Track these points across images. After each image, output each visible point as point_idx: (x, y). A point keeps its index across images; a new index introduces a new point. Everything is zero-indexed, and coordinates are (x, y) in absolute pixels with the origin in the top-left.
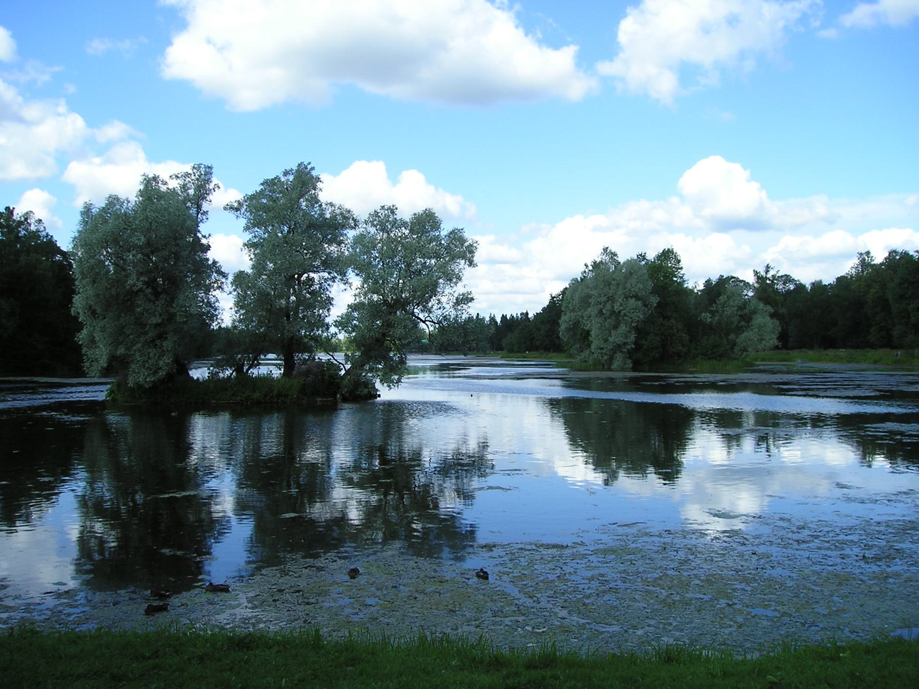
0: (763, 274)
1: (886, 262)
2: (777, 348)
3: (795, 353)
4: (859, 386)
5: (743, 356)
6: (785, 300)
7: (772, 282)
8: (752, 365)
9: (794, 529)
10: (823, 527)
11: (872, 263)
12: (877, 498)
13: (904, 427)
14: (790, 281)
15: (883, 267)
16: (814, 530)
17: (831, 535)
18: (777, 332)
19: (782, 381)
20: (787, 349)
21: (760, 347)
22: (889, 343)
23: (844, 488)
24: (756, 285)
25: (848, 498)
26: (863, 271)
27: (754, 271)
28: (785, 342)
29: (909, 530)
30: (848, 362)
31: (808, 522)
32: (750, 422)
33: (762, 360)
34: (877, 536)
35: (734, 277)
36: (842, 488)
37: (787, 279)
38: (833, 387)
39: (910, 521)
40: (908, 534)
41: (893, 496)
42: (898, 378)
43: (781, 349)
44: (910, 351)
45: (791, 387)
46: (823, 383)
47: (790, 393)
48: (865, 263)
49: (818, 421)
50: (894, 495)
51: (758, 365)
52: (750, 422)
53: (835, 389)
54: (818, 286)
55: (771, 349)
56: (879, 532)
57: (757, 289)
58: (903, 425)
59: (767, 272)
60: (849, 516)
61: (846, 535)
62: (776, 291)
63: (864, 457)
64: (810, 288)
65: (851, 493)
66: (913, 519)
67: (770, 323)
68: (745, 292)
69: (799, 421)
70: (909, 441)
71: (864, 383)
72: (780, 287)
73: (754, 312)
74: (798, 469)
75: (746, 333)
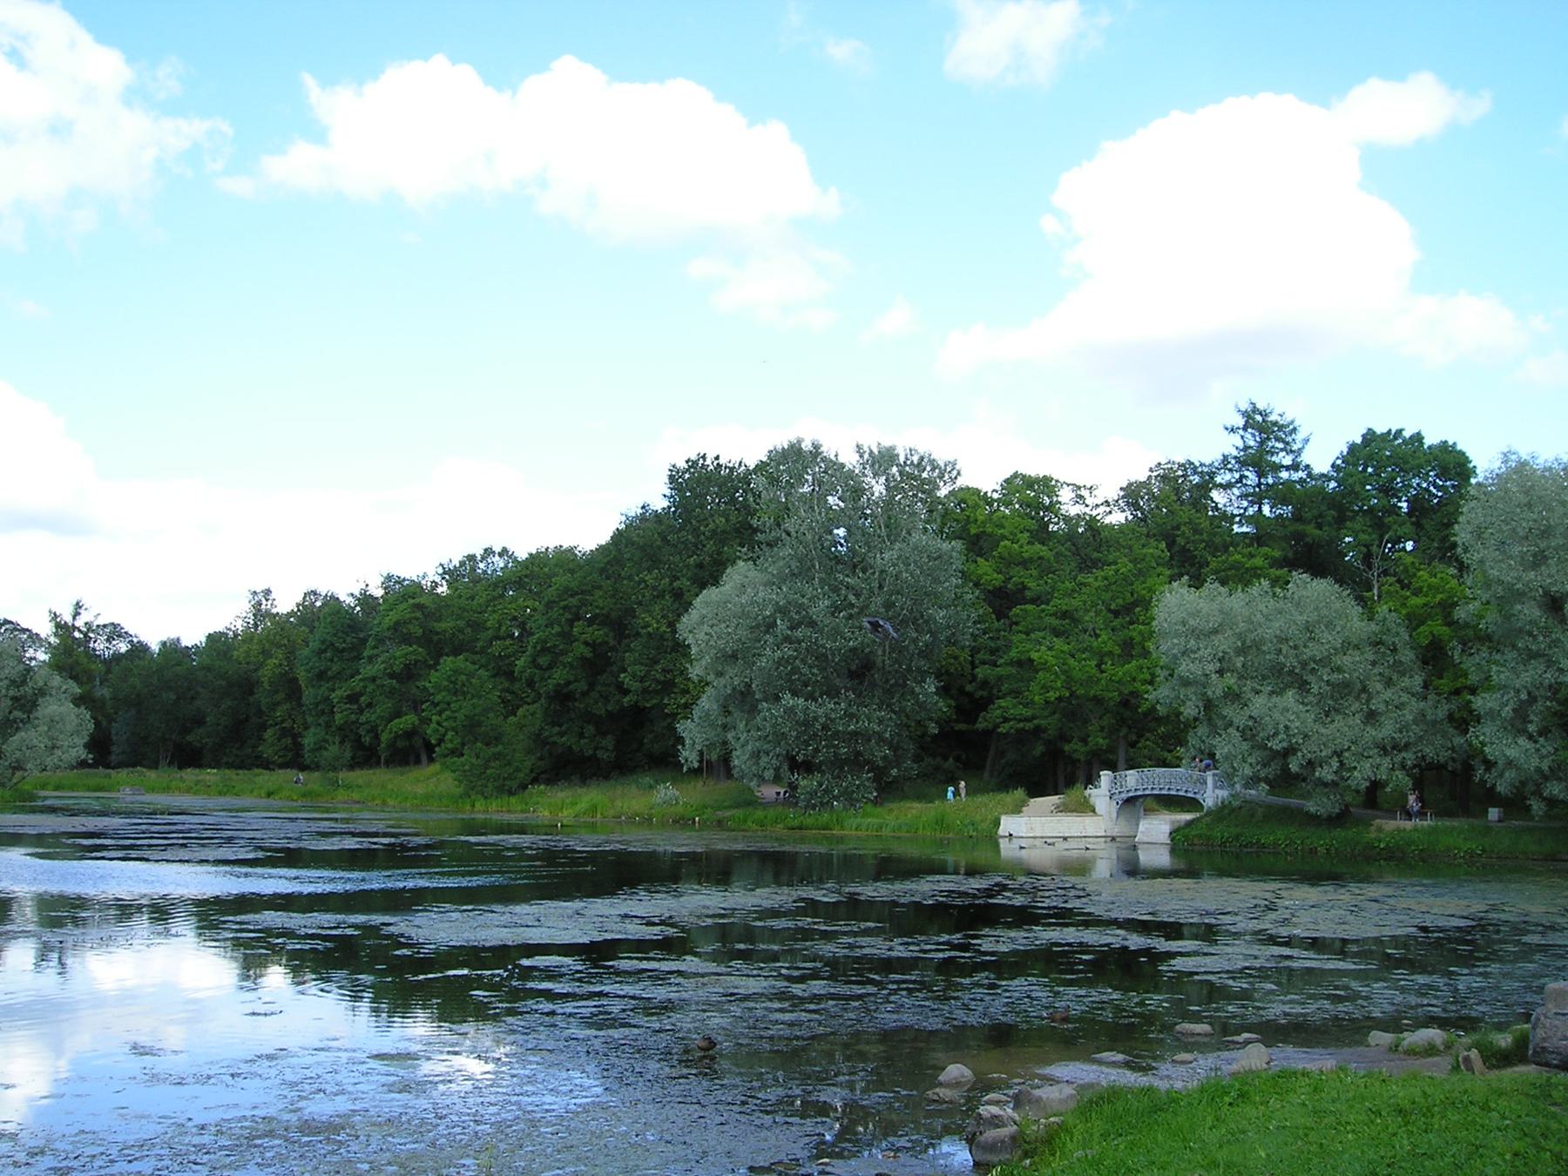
0: (67, 618)
1: (299, 610)
2: (83, 764)
3: (122, 775)
4: (230, 840)
5: (15, 781)
6: (109, 671)
7: (86, 635)
8: (33, 798)
9: (21, 1157)
10: (85, 1145)
11: (274, 611)
12: (211, 1073)
13: (294, 920)
14: (119, 636)
15: (292, 619)
16: (64, 1155)
17: (98, 1163)
18: (85, 733)
19: (84, 829)
20: (107, 766)
21: (49, 761)
22: (295, 760)
23: (147, 1054)
24: (53, 640)
25: (153, 1076)
26: (256, 626)
27: (50, 612)
28: (101, 752)
29: (259, 1137)
30: (221, 793)
31: (56, 1136)
32: (27, 915)
33: (57, 788)
34: (192, 1158)
35: (12, 623)
36: (142, 1054)
37: (115, 632)
38: (181, 841)
39: (264, 1119)
40: (256, 1146)
41: (242, 1065)
42: (304, 826)
43: (90, 766)
44: (331, 774)
45: (99, 842)
46: (164, 835)
47: (93, 855)
48: (259, 610)
49: (161, 911)
50: (247, 1062)
51: (46, 798)
52: (27, 915)
53: (184, 845)
54: (172, 649)
55: (72, 768)
56: (200, 1148)
57: (55, 648)
58: (295, 915)
59: (76, 615)
60: (143, 1117)
61: (130, 1161)
62: (92, 656)
63: (246, 978)
64: (157, 651)
65: (161, 1064)
66: (272, 1112)
67: (73, 716)
68: (30, 653)
69: (125, 910)
70: (298, 947)
71: (243, 834)
72: (100, 645)
73: (42, 692)
74: (127, 997)
75: (23, 734)
